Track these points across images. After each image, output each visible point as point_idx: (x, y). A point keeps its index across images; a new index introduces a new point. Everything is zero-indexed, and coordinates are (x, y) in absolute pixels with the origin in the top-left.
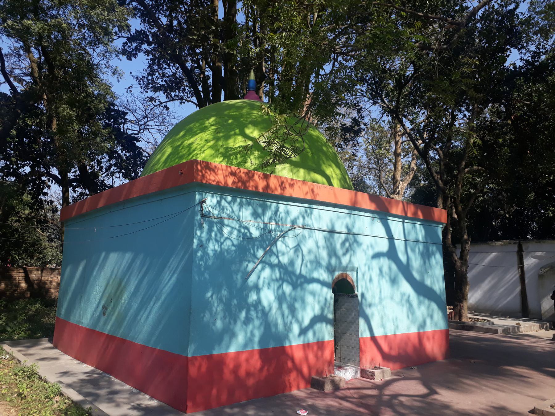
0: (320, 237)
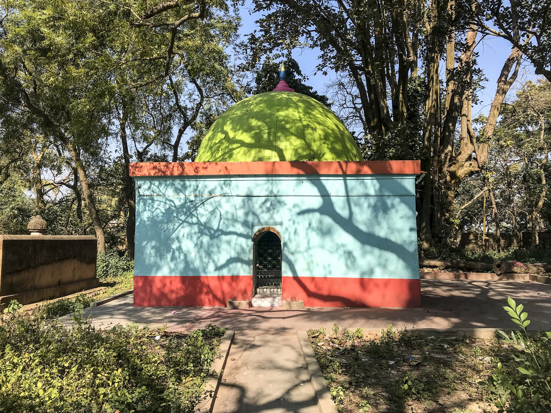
0: (238, 201)
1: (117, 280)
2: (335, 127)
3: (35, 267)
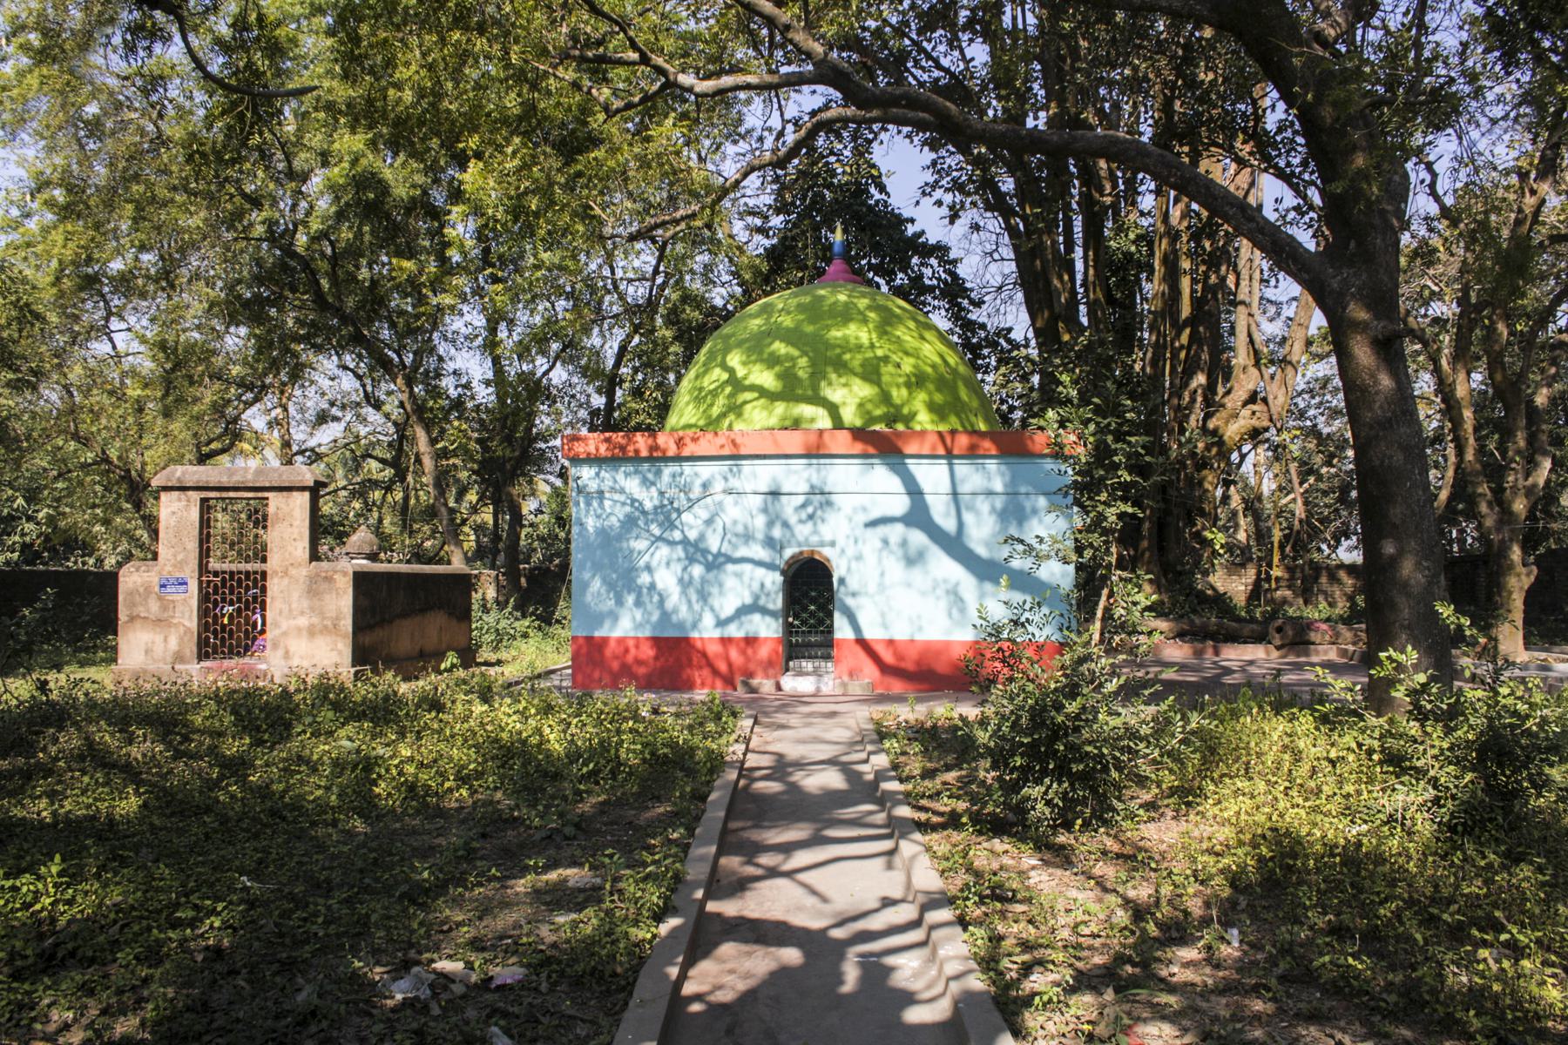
1: (503, 655)
2: (938, 360)
3: (391, 622)
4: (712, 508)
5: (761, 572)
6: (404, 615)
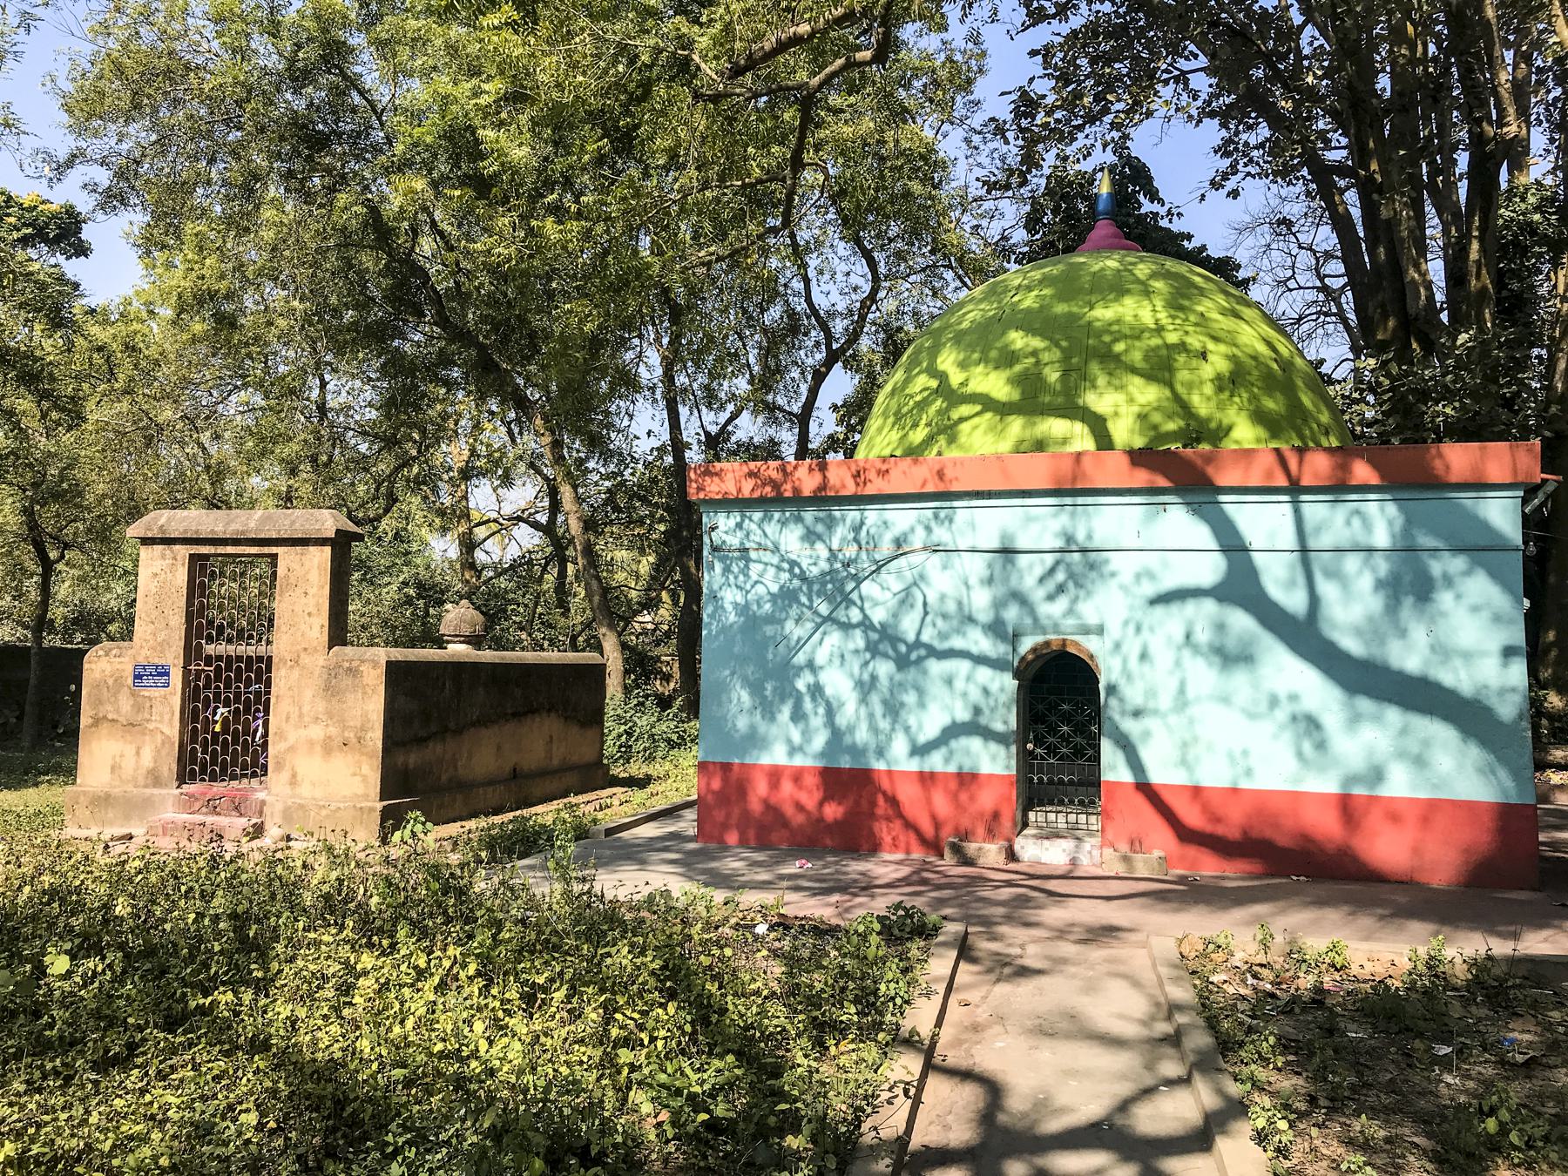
0: (976, 566)
1: (654, 769)
2: (1262, 348)
3: (459, 732)
4: (908, 575)
5: (984, 674)
6: (483, 722)
